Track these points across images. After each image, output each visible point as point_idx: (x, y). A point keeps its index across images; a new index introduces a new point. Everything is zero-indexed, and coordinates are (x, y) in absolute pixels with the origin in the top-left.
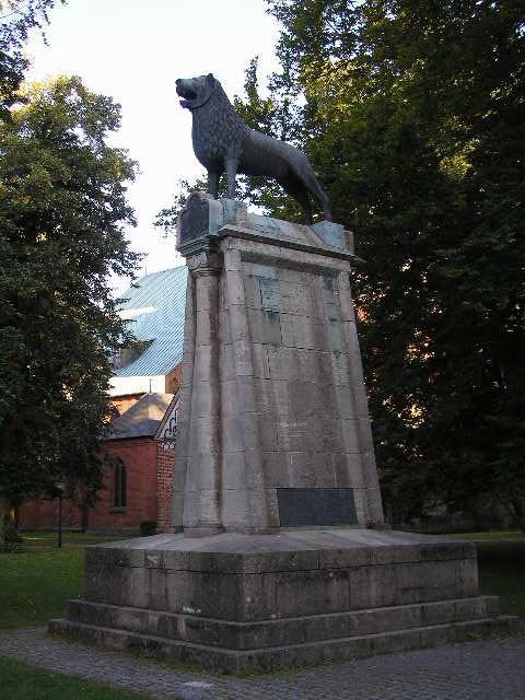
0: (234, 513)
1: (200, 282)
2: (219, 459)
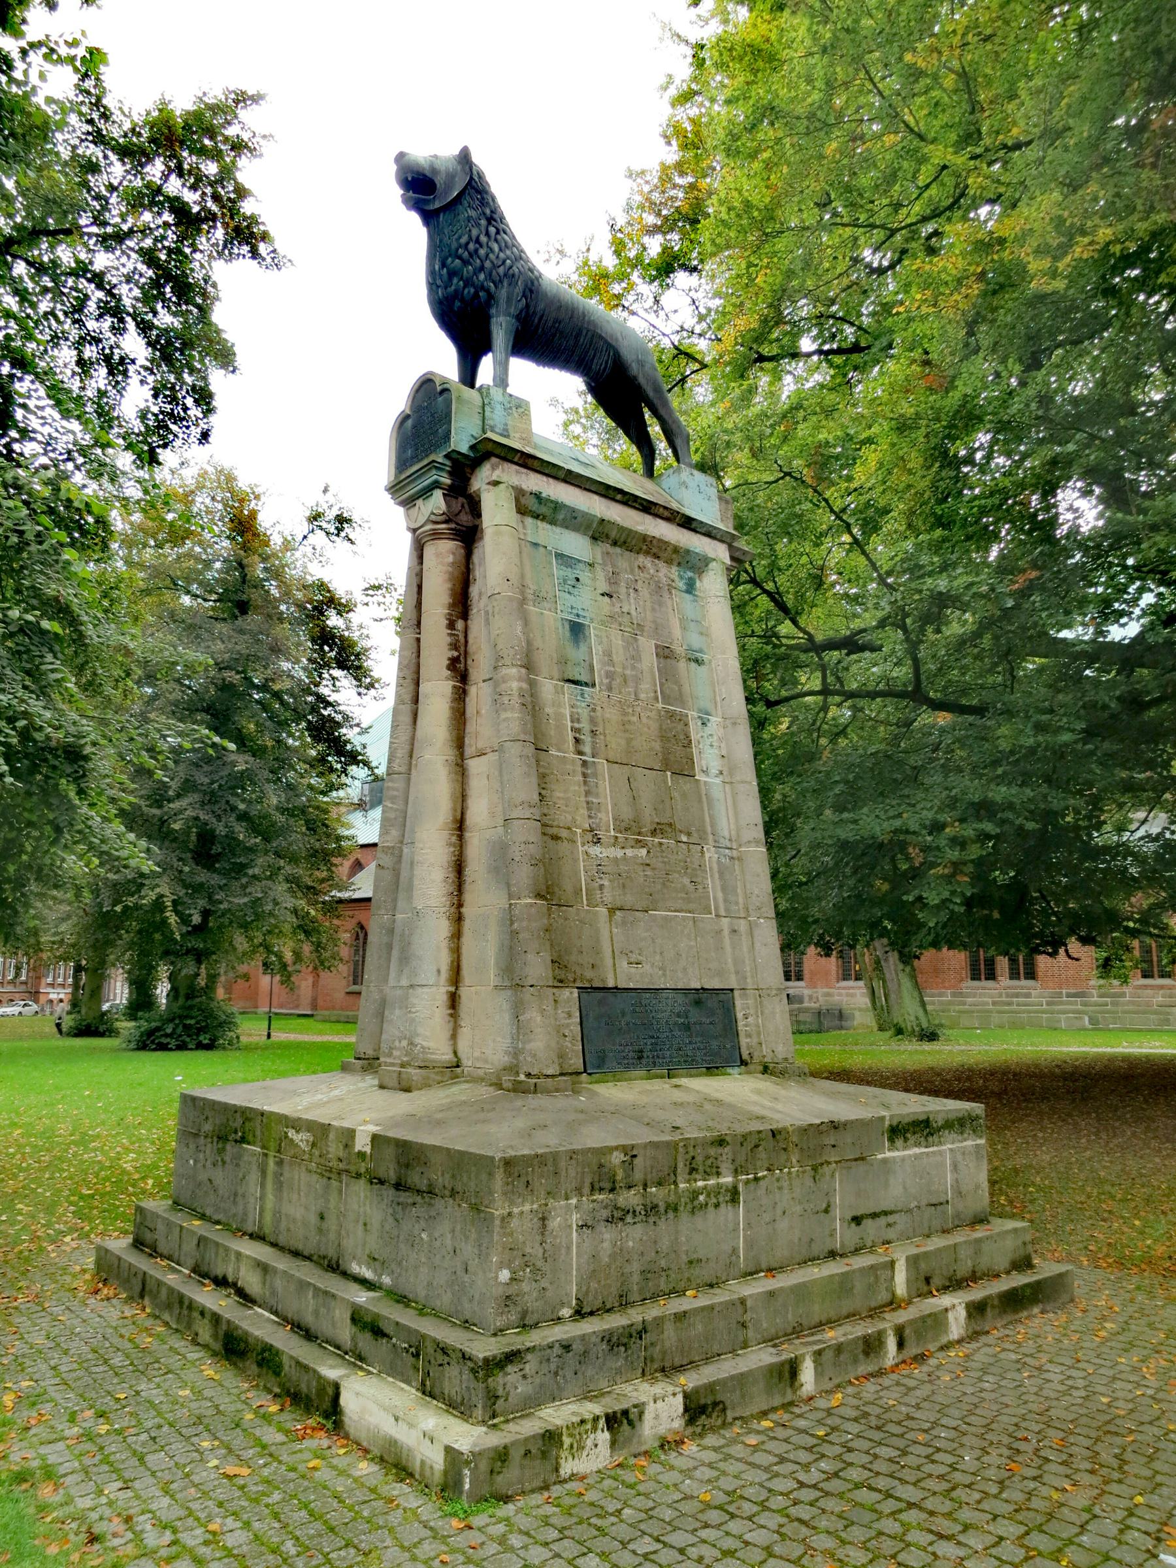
0: (487, 1040)
1: (429, 551)
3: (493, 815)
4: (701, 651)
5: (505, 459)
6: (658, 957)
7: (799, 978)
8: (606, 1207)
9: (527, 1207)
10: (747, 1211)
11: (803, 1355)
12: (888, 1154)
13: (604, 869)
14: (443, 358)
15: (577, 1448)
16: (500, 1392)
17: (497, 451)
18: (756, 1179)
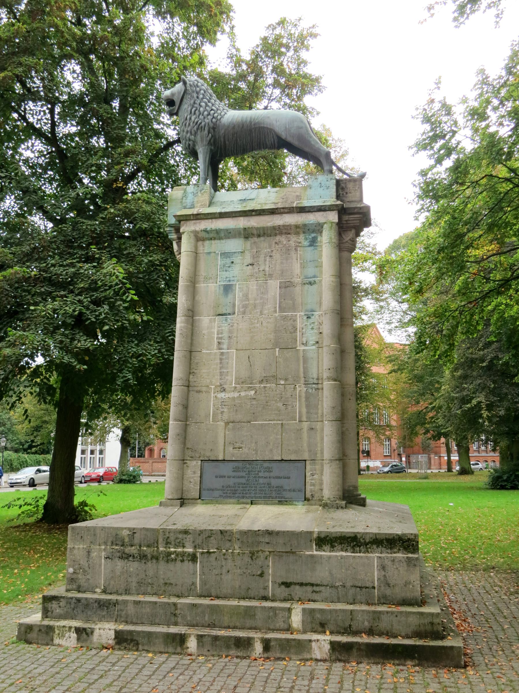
4: (315, 277)
5: (186, 220)
6: (253, 445)
8: (119, 552)
9: (81, 546)
10: (202, 567)
11: (190, 635)
12: (315, 553)
13: (226, 404)
15: (62, 636)
16: (50, 609)
17: (182, 219)
18: (209, 553)
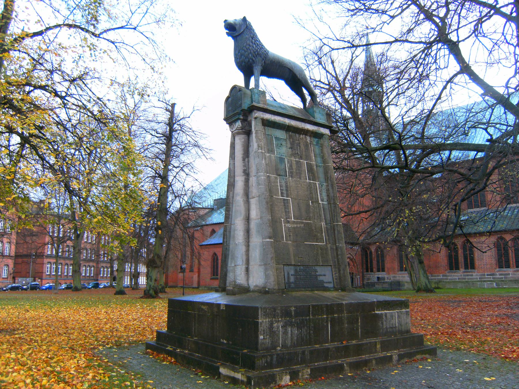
2: (248, 246)
3: (257, 215)
7: (383, 270)
14: (239, 79)
